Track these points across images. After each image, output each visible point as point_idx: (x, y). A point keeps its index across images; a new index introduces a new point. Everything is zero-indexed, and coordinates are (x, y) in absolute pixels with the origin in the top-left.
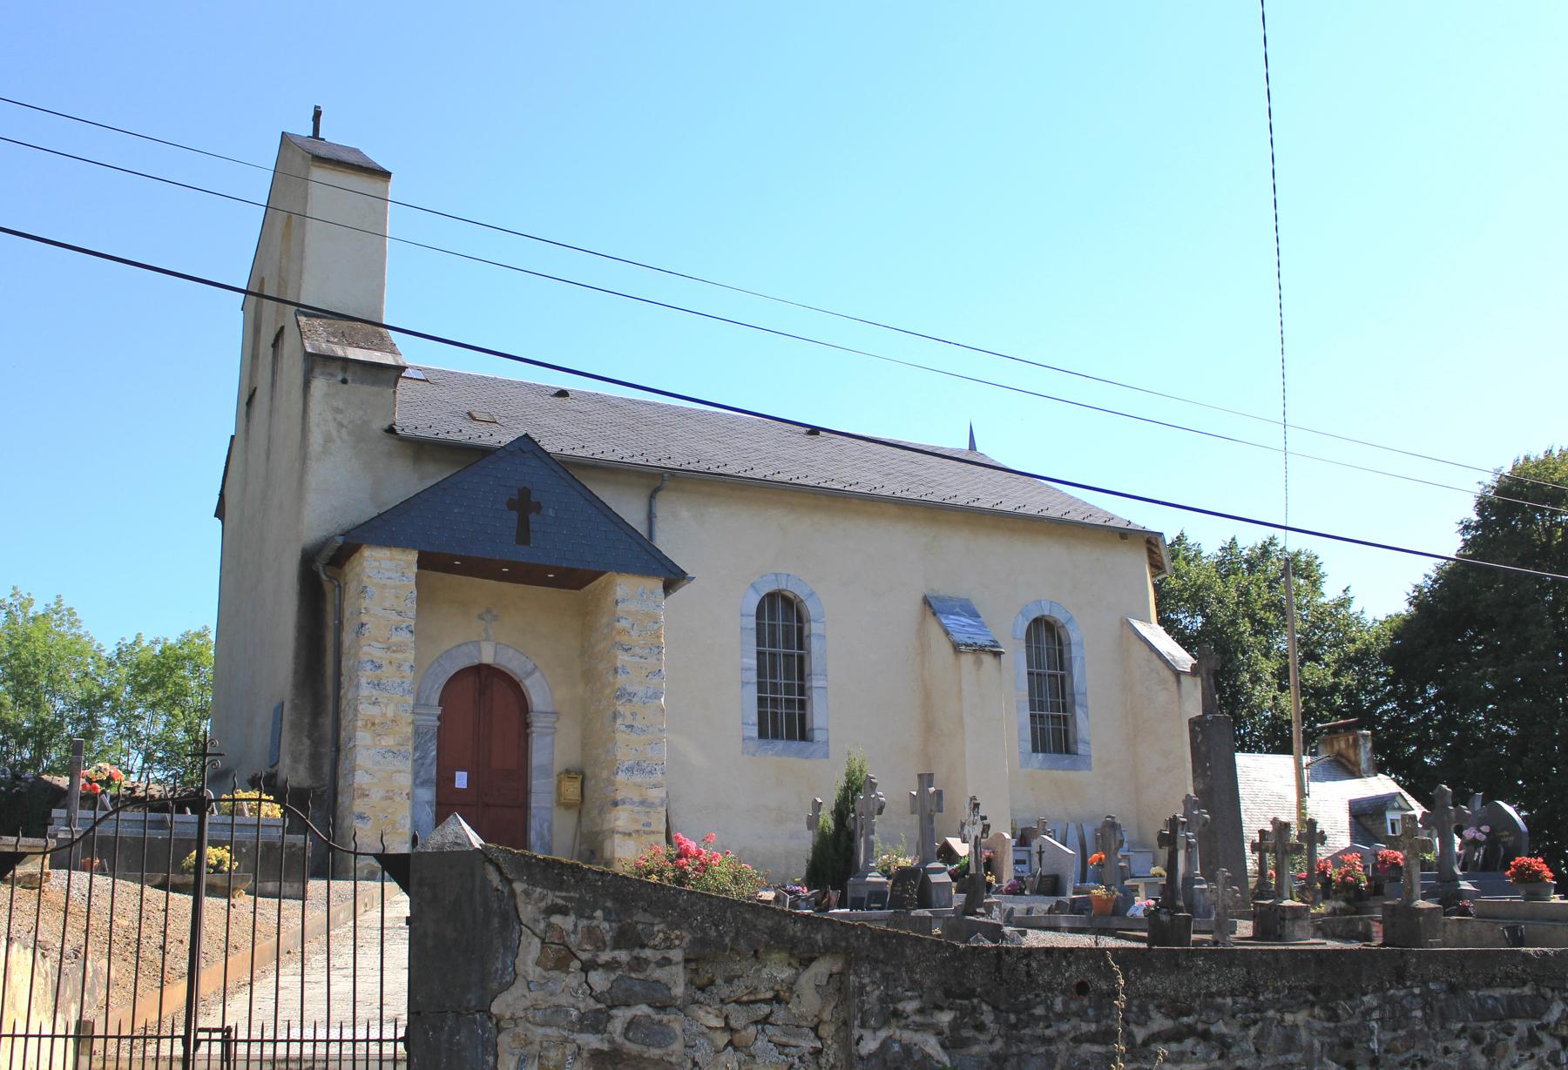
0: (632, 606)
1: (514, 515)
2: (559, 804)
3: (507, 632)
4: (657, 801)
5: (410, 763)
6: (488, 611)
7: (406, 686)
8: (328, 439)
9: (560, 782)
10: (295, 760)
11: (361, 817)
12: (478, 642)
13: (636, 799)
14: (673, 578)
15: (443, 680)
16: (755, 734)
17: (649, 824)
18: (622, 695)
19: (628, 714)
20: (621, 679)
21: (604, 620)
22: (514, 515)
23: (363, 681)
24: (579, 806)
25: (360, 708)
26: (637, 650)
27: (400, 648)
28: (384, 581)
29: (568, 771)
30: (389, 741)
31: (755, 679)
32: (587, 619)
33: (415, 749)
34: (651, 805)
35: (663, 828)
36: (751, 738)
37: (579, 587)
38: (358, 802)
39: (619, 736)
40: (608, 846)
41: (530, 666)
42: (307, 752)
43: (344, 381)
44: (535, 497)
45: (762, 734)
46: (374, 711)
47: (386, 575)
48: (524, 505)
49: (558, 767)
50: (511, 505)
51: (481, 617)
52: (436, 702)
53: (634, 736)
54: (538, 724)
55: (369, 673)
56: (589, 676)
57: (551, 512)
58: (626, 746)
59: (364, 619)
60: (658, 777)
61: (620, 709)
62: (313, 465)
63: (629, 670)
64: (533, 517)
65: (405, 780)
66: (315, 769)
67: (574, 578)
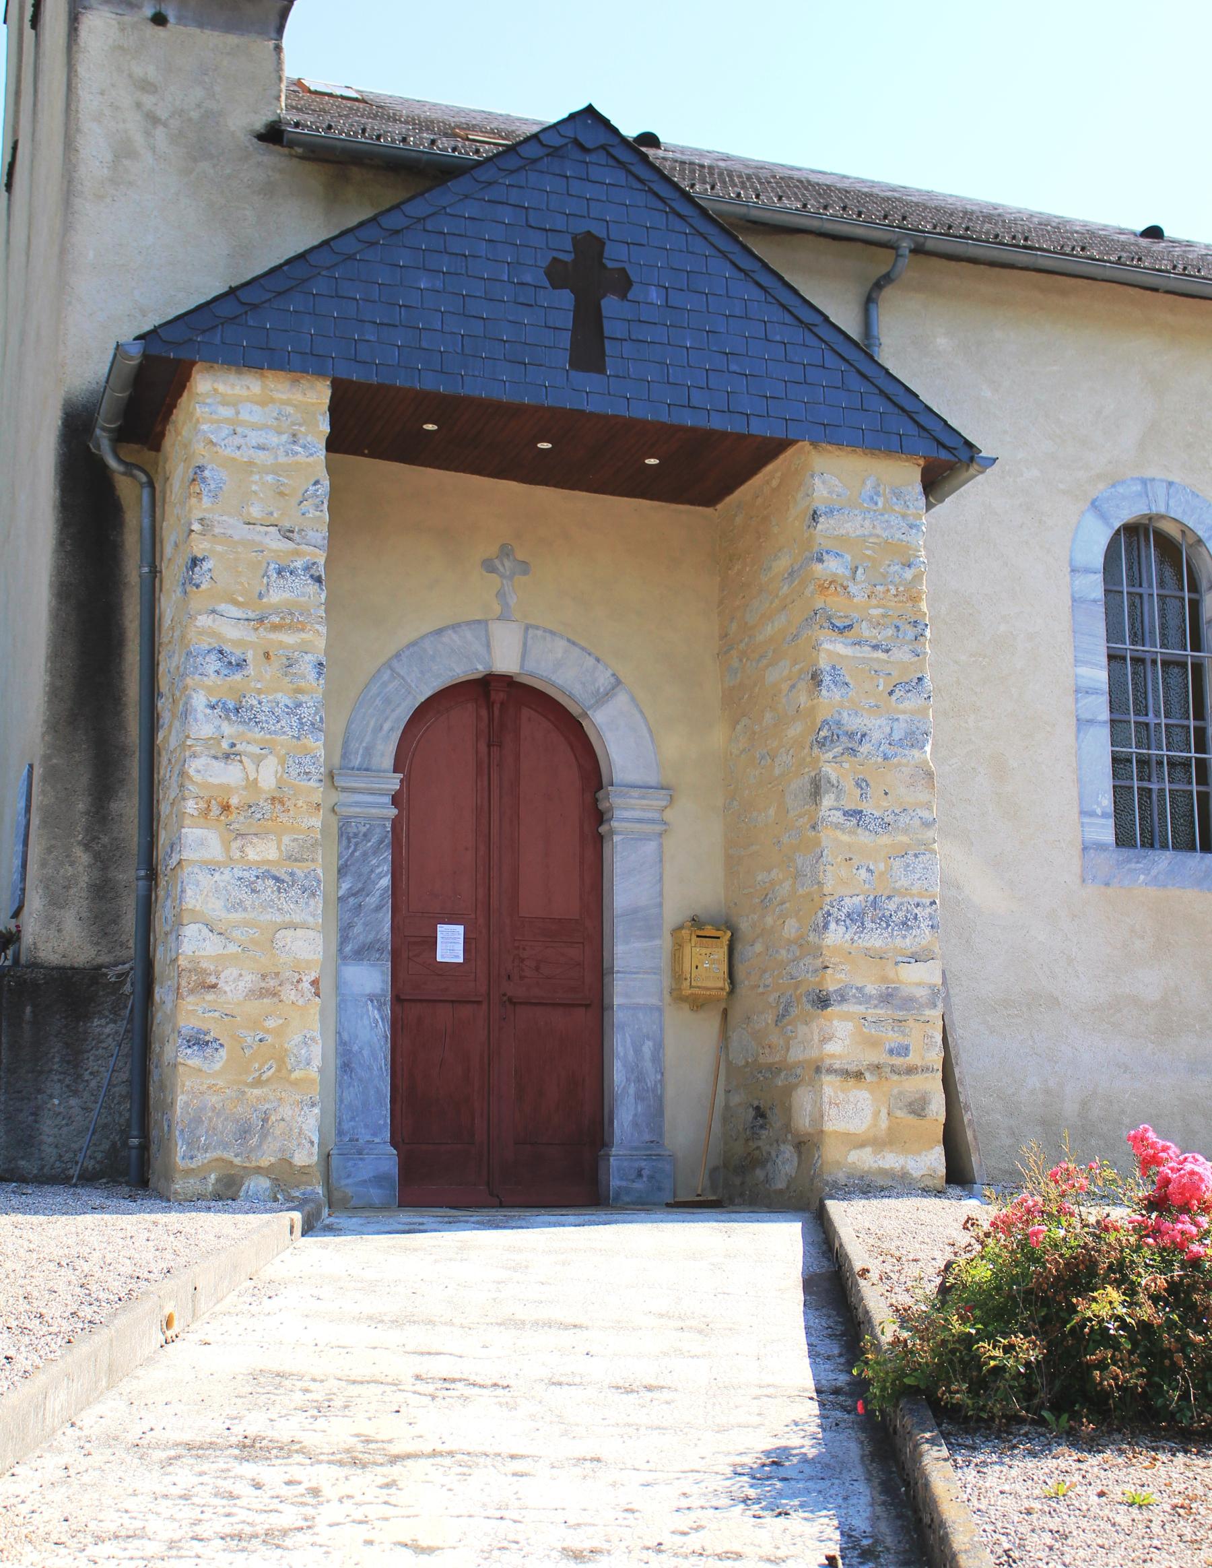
0: (853, 526)
1: (566, 298)
2: (679, 997)
3: (550, 597)
4: (922, 993)
5: (317, 904)
6: (505, 551)
7: (305, 712)
8: (123, 151)
9: (678, 947)
10: (55, 901)
11: (198, 1041)
12: (486, 622)
13: (871, 989)
14: (946, 461)
15: (404, 712)
16: (1109, 836)
17: (904, 1050)
18: (833, 739)
19: (848, 784)
20: (830, 696)
21: (782, 563)
22: (566, 298)
23: (199, 701)
24: (726, 1004)
25: (193, 767)
26: (865, 631)
27: (290, 619)
28: (243, 456)
29: (696, 922)
30: (264, 851)
31: (1105, 715)
32: (732, 574)
33: (342, 871)
34: (908, 1003)
35: (935, 1057)
36: (1101, 847)
37: (711, 498)
38: (190, 1003)
39: (827, 837)
40: (803, 1101)
41: (603, 679)
42: (84, 880)
43: (159, 20)
44: (615, 256)
45: (1123, 839)
46: (229, 775)
47: (253, 438)
48: (588, 275)
49: (672, 915)
50: (557, 275)
51: (489, 566)
52: (388, 762)
53: (864, 838)
54: (626, 814)
55: (212, 680)
56: (741, 702)
57: (654, 295)
58: (846, 866)
59: (199, 546)
60: (922, 936)
61: (830, 770)
62: (87, 209)
63: (848, 673)
64: (610, 305)
65: (307, 945)
66: (102, 922)
67: (702, 467)
